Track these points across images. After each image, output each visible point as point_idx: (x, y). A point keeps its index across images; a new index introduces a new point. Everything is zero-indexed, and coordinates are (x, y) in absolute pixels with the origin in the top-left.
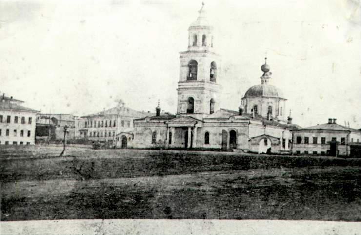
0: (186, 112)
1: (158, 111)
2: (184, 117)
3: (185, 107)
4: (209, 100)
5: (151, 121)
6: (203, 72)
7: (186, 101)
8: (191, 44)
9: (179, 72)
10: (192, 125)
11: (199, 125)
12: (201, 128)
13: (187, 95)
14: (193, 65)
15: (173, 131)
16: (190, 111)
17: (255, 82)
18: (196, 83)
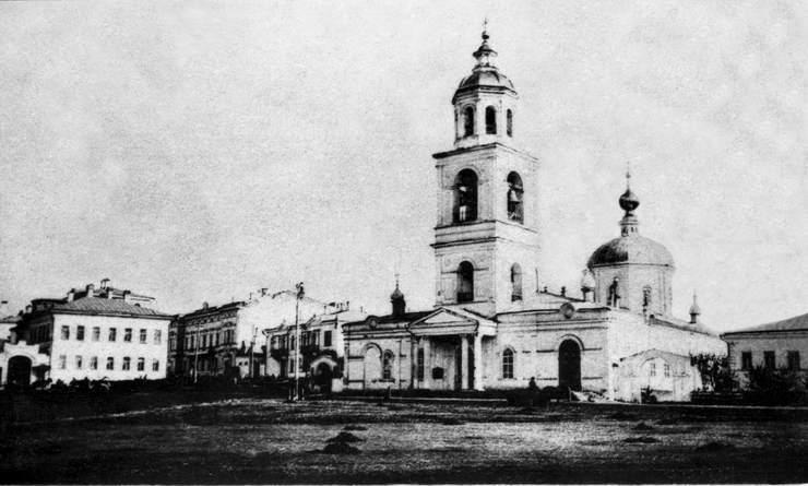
0: (455, 301)
1: (398, 301)
2: (449, 311)
3: (452, 284)
4: (509, 267)
5: (378, 327)
6: (493, 196)
7: (454, 272)
8: (462, 132)
10: (470, 330)
11: (486, 328)
12: (493, 338)
13: (456, 256)
14: (467, 182)
15: (426, 346)
16: (465, 297)
17: (607, 231)
18: (480, 226)
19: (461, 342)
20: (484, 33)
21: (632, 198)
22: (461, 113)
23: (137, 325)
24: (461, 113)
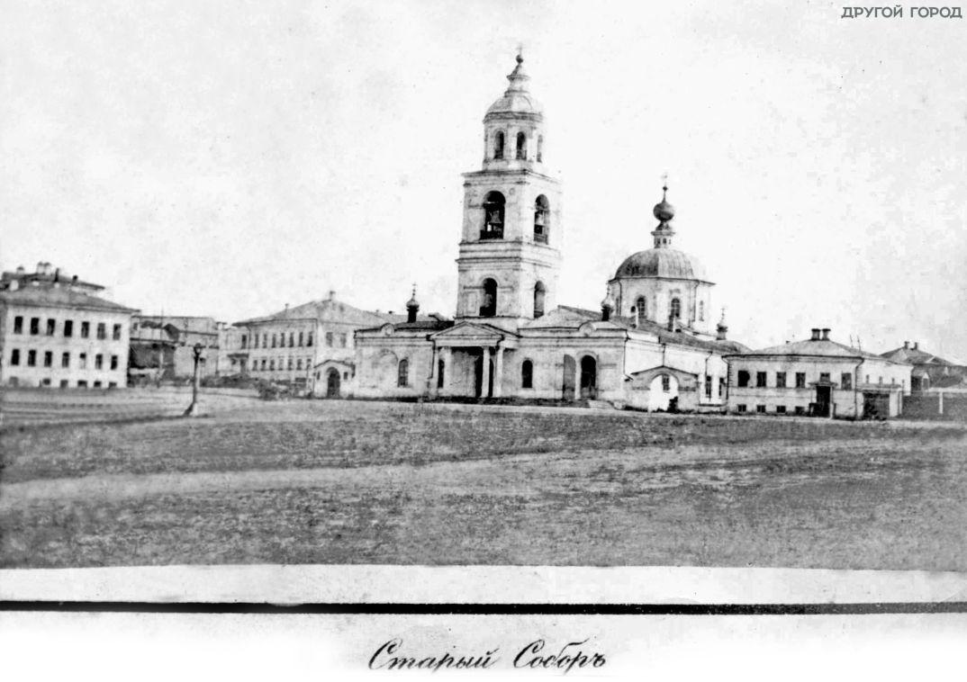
3: (477, 300)
6: (519, 220)
8: (492, 155)
9: (453, 218)
10: (493, 343)
12: (512, 350)
13: (478, 274)
14: (495, 204)
15: (448, 357)
16: (489, 311)
17: (640, 243)
19: (483, 353)
20: (518, 56)
21: (561, 361)
22: (492, 137)
23: (94, 319)
24: (492, 137)
